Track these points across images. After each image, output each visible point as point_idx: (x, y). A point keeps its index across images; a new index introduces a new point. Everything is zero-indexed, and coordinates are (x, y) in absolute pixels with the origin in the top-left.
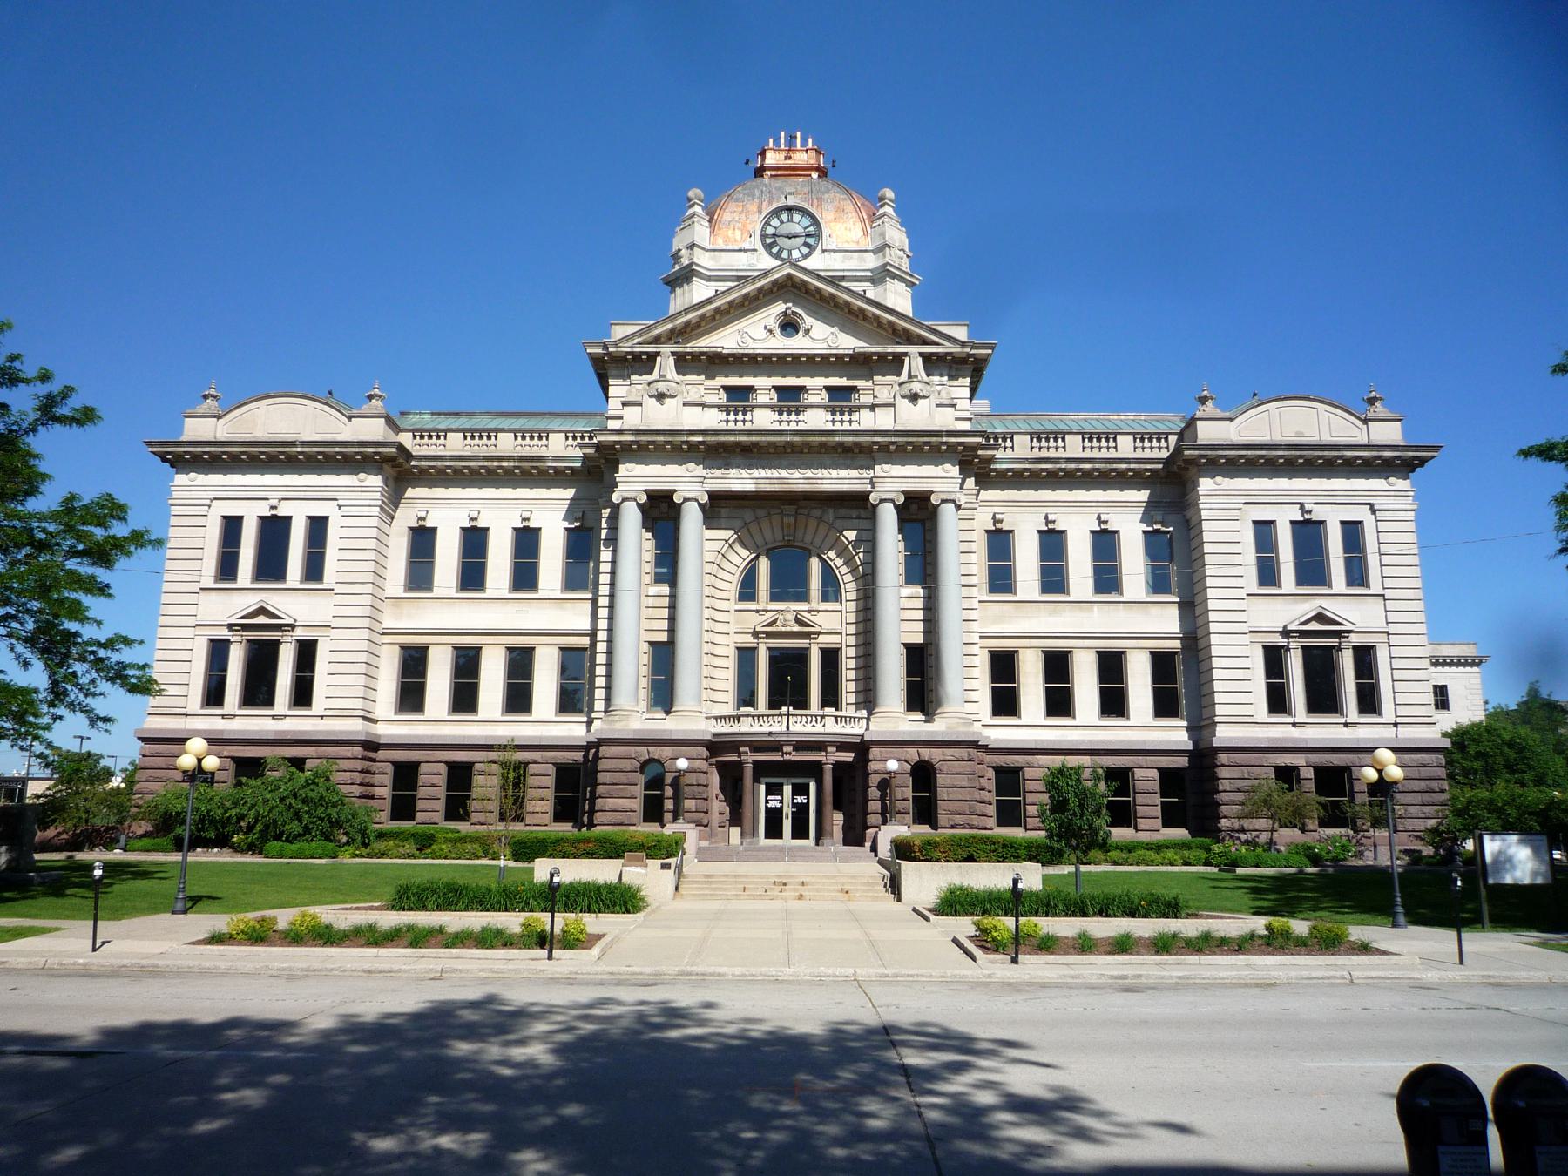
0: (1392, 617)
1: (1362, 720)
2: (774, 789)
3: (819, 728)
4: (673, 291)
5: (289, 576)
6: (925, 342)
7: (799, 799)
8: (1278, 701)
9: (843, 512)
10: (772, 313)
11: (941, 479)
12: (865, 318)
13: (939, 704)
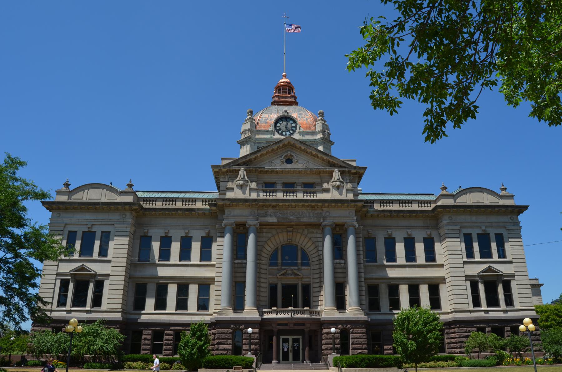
0: (462, 270)
1: (199, 312)
2: (286, 341)
4: (241, 147)
5: (171, 258)
6: (341, 166)
7: (295, 344)
12: (318, 157)
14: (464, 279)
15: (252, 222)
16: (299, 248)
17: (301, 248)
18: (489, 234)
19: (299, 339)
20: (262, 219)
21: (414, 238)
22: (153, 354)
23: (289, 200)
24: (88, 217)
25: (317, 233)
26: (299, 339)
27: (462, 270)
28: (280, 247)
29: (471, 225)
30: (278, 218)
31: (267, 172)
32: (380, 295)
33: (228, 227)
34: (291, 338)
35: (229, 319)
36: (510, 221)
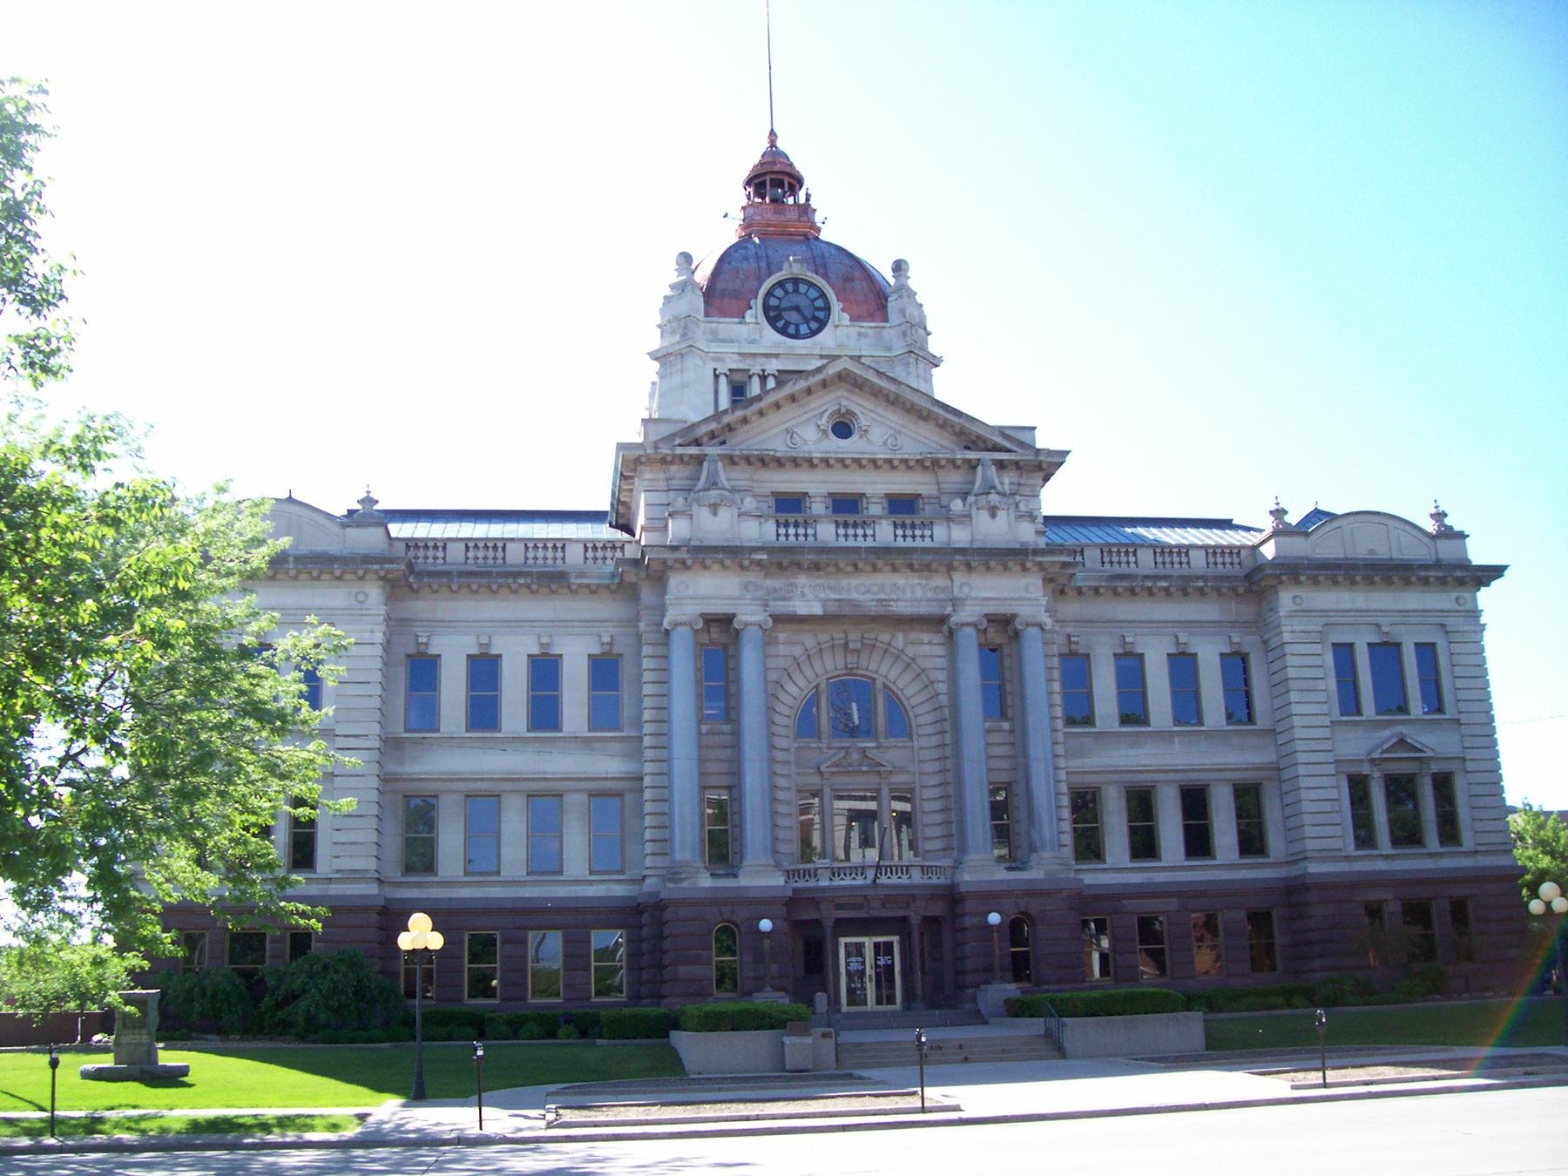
0: (1468, 742)
3: (905, 880)
8: (1365, 838)
9: (914, 635)
10: (827, 404)
11: (1021, 593)
13: (741, 854)
14: (1331, 769)
15: (750, 614)
16: (879, 686)
17: (885, 685)
18: (1398, 645)
19: (890, 944)
20: (780, 607)
21: (1195, 655)
22: (159, 1040)
23: (914, 550)
24: (1381, 600)
25: (930, 643)
26: (890, 944)
27: (1328, 745)
28: (823, 686)
29: (1351, 620)
30: (824, 602)
31: (779, 463)
32: (1106, 819)
33: (681, 629)
34: (868, 942)
35: (771, 894)
36: (1457, 607)
